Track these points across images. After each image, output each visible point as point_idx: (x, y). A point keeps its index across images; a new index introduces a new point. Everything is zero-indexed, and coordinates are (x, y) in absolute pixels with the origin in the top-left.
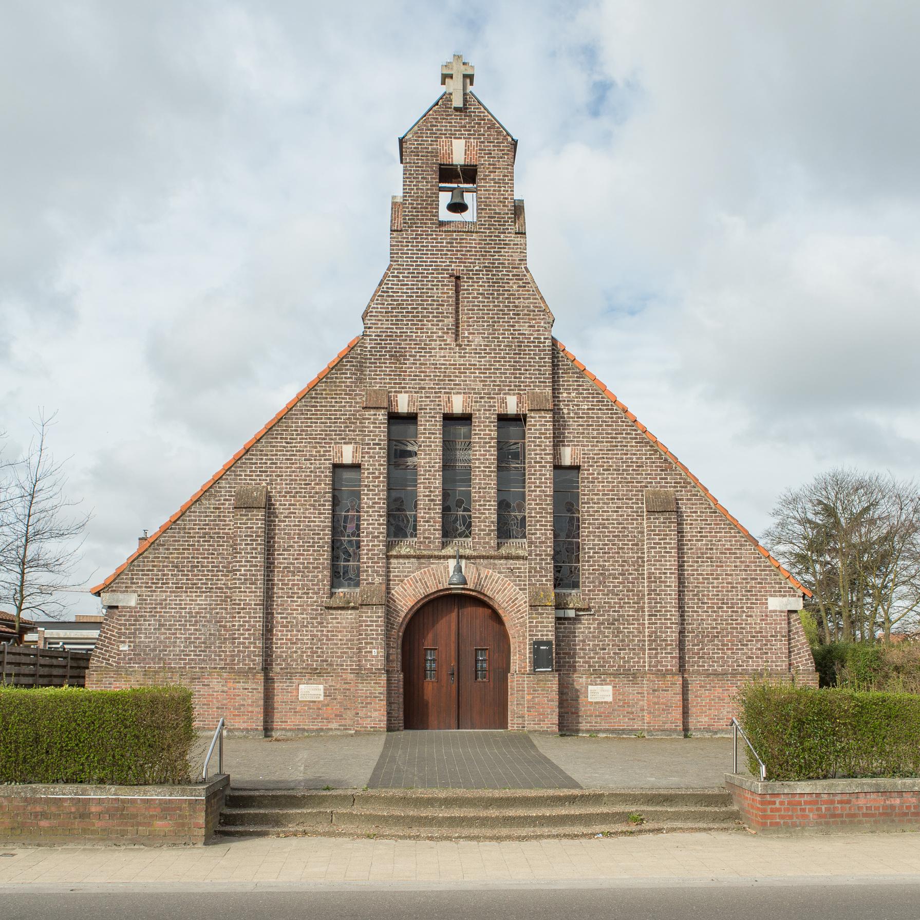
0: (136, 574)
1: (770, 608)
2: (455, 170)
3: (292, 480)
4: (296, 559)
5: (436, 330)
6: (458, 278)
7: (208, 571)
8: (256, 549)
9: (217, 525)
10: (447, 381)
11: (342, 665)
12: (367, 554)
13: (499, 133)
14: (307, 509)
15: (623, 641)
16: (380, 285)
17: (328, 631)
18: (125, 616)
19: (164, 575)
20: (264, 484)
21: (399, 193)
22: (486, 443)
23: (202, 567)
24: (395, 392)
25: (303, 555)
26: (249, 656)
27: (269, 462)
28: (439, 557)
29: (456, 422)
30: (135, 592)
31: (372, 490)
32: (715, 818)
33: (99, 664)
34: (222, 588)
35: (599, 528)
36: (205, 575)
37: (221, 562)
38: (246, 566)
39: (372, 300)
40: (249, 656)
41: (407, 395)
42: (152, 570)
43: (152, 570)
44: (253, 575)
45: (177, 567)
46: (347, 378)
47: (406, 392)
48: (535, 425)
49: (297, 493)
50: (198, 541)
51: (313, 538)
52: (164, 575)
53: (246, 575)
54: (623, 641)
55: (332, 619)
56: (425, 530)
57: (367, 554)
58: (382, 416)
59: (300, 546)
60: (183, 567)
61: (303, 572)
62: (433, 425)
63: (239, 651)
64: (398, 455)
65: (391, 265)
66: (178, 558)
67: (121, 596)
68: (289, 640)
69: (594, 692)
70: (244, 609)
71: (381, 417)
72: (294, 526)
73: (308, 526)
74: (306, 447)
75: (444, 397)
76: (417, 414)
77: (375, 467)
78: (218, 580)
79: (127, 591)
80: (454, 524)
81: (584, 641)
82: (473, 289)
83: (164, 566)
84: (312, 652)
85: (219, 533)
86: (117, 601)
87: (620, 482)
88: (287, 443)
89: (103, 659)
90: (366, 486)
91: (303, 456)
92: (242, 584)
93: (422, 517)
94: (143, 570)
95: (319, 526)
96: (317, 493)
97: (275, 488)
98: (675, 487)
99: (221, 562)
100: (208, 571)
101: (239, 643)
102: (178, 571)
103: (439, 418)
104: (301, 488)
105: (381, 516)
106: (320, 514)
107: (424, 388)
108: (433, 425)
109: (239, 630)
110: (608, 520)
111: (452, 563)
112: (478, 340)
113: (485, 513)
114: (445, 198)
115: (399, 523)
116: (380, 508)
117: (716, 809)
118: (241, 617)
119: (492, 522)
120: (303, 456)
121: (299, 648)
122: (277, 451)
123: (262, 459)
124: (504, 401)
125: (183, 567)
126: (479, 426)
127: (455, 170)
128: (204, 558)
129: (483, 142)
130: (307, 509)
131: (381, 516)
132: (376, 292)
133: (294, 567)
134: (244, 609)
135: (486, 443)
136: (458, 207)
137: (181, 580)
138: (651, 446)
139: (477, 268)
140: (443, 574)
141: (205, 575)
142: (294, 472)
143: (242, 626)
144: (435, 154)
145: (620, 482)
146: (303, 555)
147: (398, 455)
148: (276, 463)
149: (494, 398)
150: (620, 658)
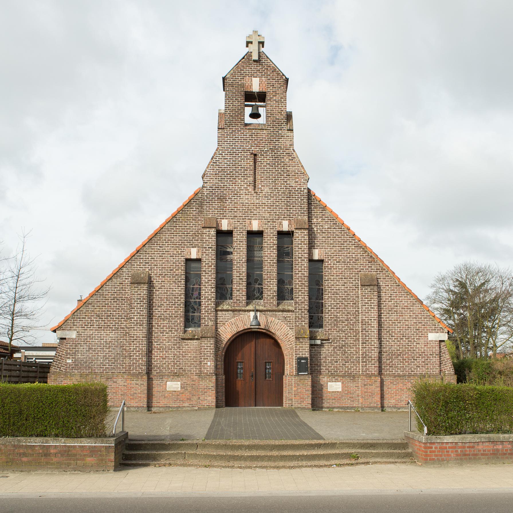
0: (76, 320)
1: (430, 339)
2: (254, 94)
3: (163, 268)
4: (165, 312)
5: (243, 184)
6: (255, 155)
7: (116, 318)
8: (143, 306)
9: (121, 293)
10: (249, 213)
11: (191, 371)
12: (205, 309)
13: (278, 74)
14: (171, 284)
15: (347, 357)
16: (212, 159)
17: (183, 352)
18: (69, 343)
19: (91, 321)
20: (147, 270)
21: (223, 108)
22: (271, 247)
23: (113, 316)
24: (220, 218)
25: (169, 309)
26: (139, 366)
27: (150, 258)
28: (245, 311)
29: (254, 236)
30: (75, 330)
31: (207, 273)
32: (399, 456)
33: (55, 370)
34: (124, 328)
35: (334, 294)
36: (114, 321)
37: (123, 314)
38: (137, 316)
39: (207, 167)
40: (139, 366)
41: (227, 220)
42: (85, 318)
43: (85, 318)
44: (141, 321)
45: (98, 316)
46: (193, 211)
47: (226, 219)
48: (298, 237)
49: (165, 275)
50: (111, 302)
51: (175, 300)
52: (91, 321)
53: (137, 321)
54: (347, 357)
55: (185, 345)
56: (237, 296)
57: (205, 309)
58: (213, 232)
59: (167, 305)
60: (102, 316)
61: (169, 319)
62: (241, 237)
63: (133, 363)
64: (222, 254)
65: (218, 148)
66: (99, 311)
67: (67, 332)
68: (161, 357)
69: (331, 386)
70: (136, 339)
71: (212, 233)
72: (164, 293)
73: (172, 293)
74: (171, 249)
75: (248, 221)
76: (232, 231)
77: (209, 260)
78: (121, 323)
79: (71, 330)
80: (253, 292)
81: (325, 357)
82: (264, 161)
83: (91, 316)
84: (174, 364)
85: (122, 297)
86: (66, 335)
87: (346, 269)
88: (160, 247)
89: (58, 367)
90: (204, 271)
91: (169, 254)
92: (135, 325)
93: (235, 288)
94: (80, 318)
95: (178, 293)
96: (177, 275)
97: (154, 272)
98: (376, 272)
99: (123, 314)
100: (116, 318)
101: (133, 359)
102: (99, 318)
103: (245, 233)
104: (168, 272)
105: (212, 288)
106: (178, 286)
107: (236, 217)
108: (241, 237)
109: (133, 351)
110: (339, 290)
111: (252, 314)
112: (266, 189)
113: (270, 286)
114: (248, 111)
115: (223, 292)
116: (212, 283)
117: (399, 451)
118: (134, 344)
119: (275, 291)
120: (169, 254)
121: (167, 361)
122: (154, 251)
123: (146, 256)
124: (281, 224)
125: (102, 316)
126: (267, 238)
127: (254, 94)
128: (114, 311)
129: (269, 79)
130: (171, 284)
131: (212, 288)
132: (210, 163)
133: (164, 316)
134: (136, 339)
135: (271, 247)
136: (255, 115)
137: (101, 323)
138: (363, 249)
139: (266, 149)
140: (247, 320)
141: (114, 321)
142: (164, 263)
143: (135, 349)
144: (243, 86)
145: (346, 269)
146: (169, 309)
147: (222, 254)
148: (154, 258)
149: (275, 222)
150: (346, 367)
